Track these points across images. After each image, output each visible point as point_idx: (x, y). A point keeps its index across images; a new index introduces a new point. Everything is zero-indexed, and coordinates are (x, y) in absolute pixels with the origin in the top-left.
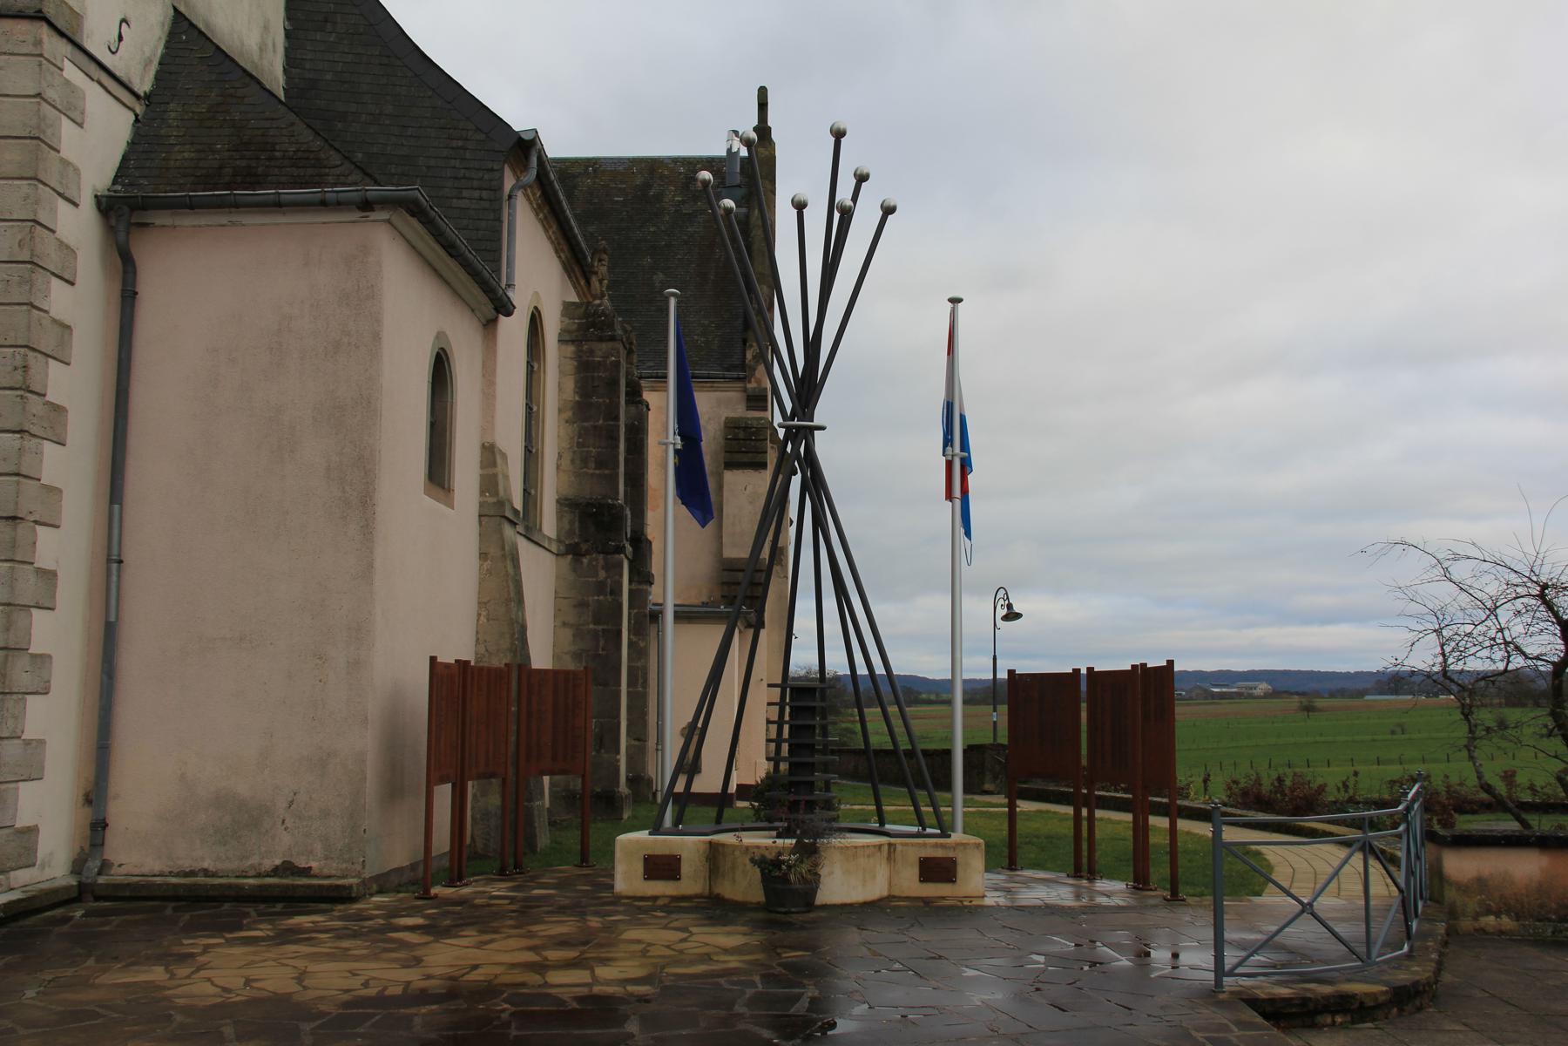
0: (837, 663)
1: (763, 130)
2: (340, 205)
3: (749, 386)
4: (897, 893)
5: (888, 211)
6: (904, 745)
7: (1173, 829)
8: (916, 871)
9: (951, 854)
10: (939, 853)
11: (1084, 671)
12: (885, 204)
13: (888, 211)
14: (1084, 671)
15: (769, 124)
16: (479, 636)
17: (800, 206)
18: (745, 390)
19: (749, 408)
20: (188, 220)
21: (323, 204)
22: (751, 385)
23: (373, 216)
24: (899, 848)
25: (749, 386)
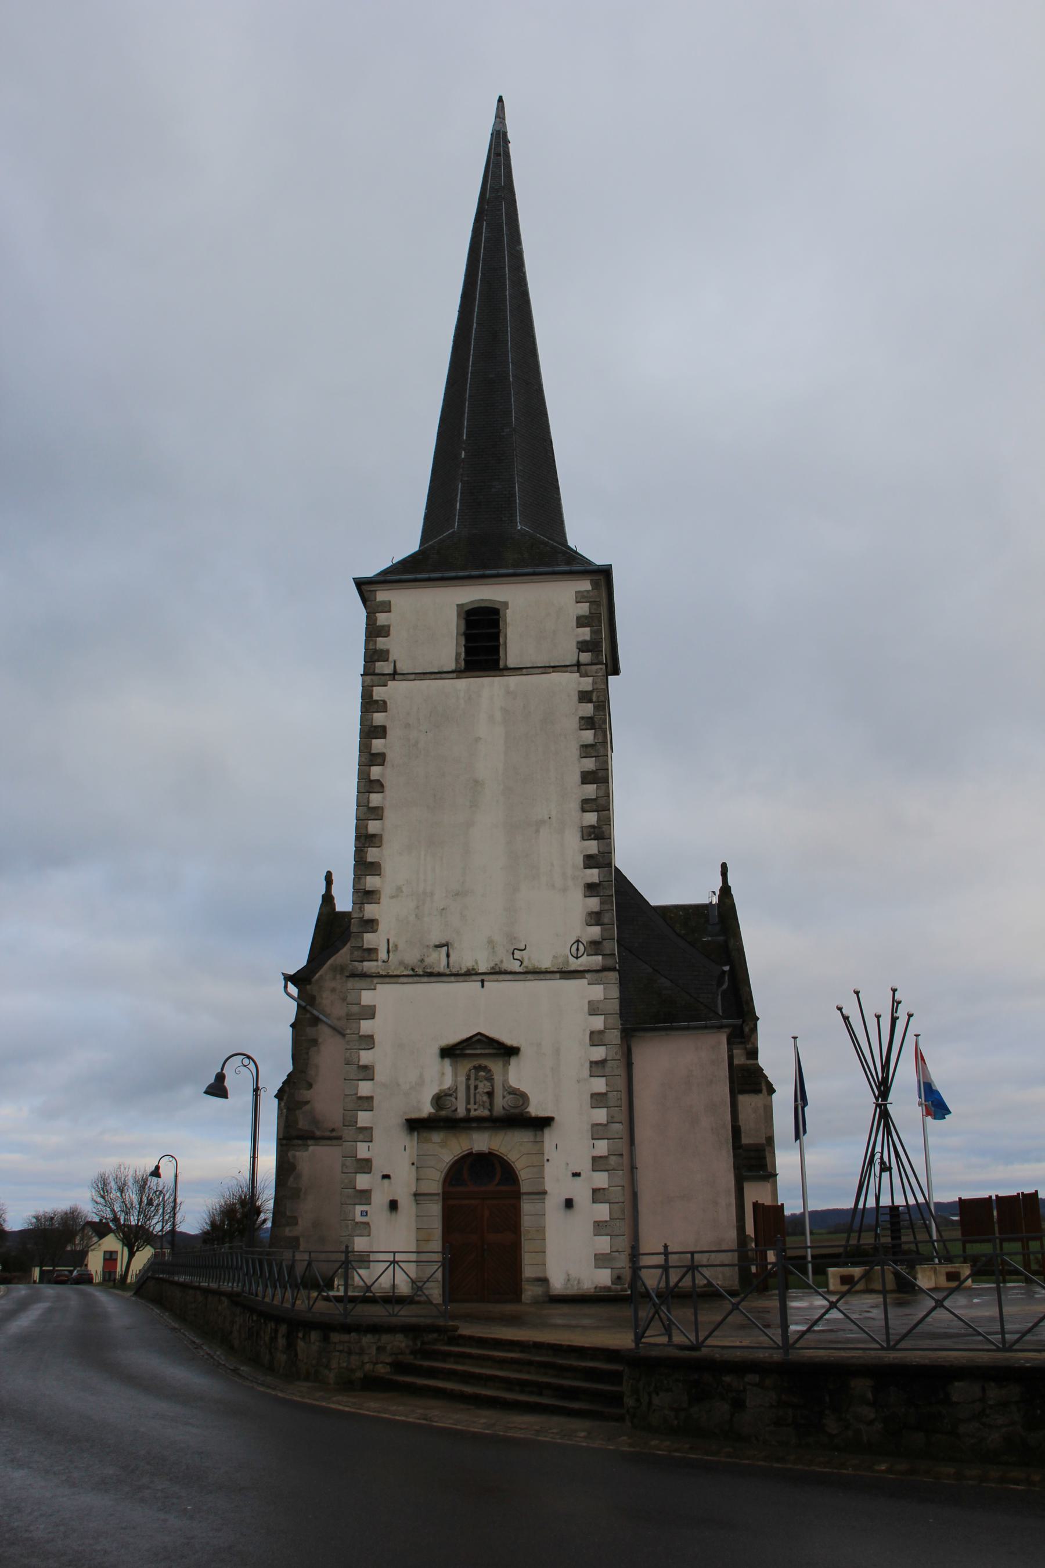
0: (899, 1201)
1: (726, 891)
2: (712, 1027)
3: (748, 1046)
4: (938, 1286)
5: (910, 1016)
6: (413, 1257)
7: (670, 1337)
8: (945, 1277)
9: (958, 1270)
10: (953, 1270)
11: (994, 1198)
12: (909, 1013)
13: (910, 1016)
14: (994, 1198)
15: (729, 884)
16: (601, 1191)
17: (878, 1017)
18: (746, 1049)
19: (748, 1059)
20: (649, 1034)
21: (706, 1027)
22: (749, 1046)
23: (722, 1030)
24: (938, 1268)
25: (748, 1046)
